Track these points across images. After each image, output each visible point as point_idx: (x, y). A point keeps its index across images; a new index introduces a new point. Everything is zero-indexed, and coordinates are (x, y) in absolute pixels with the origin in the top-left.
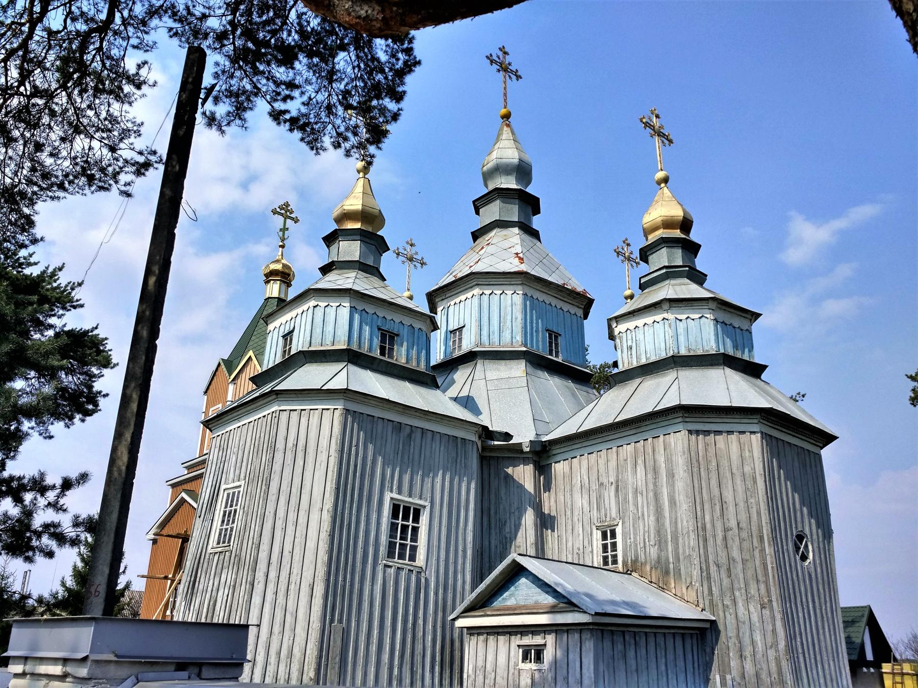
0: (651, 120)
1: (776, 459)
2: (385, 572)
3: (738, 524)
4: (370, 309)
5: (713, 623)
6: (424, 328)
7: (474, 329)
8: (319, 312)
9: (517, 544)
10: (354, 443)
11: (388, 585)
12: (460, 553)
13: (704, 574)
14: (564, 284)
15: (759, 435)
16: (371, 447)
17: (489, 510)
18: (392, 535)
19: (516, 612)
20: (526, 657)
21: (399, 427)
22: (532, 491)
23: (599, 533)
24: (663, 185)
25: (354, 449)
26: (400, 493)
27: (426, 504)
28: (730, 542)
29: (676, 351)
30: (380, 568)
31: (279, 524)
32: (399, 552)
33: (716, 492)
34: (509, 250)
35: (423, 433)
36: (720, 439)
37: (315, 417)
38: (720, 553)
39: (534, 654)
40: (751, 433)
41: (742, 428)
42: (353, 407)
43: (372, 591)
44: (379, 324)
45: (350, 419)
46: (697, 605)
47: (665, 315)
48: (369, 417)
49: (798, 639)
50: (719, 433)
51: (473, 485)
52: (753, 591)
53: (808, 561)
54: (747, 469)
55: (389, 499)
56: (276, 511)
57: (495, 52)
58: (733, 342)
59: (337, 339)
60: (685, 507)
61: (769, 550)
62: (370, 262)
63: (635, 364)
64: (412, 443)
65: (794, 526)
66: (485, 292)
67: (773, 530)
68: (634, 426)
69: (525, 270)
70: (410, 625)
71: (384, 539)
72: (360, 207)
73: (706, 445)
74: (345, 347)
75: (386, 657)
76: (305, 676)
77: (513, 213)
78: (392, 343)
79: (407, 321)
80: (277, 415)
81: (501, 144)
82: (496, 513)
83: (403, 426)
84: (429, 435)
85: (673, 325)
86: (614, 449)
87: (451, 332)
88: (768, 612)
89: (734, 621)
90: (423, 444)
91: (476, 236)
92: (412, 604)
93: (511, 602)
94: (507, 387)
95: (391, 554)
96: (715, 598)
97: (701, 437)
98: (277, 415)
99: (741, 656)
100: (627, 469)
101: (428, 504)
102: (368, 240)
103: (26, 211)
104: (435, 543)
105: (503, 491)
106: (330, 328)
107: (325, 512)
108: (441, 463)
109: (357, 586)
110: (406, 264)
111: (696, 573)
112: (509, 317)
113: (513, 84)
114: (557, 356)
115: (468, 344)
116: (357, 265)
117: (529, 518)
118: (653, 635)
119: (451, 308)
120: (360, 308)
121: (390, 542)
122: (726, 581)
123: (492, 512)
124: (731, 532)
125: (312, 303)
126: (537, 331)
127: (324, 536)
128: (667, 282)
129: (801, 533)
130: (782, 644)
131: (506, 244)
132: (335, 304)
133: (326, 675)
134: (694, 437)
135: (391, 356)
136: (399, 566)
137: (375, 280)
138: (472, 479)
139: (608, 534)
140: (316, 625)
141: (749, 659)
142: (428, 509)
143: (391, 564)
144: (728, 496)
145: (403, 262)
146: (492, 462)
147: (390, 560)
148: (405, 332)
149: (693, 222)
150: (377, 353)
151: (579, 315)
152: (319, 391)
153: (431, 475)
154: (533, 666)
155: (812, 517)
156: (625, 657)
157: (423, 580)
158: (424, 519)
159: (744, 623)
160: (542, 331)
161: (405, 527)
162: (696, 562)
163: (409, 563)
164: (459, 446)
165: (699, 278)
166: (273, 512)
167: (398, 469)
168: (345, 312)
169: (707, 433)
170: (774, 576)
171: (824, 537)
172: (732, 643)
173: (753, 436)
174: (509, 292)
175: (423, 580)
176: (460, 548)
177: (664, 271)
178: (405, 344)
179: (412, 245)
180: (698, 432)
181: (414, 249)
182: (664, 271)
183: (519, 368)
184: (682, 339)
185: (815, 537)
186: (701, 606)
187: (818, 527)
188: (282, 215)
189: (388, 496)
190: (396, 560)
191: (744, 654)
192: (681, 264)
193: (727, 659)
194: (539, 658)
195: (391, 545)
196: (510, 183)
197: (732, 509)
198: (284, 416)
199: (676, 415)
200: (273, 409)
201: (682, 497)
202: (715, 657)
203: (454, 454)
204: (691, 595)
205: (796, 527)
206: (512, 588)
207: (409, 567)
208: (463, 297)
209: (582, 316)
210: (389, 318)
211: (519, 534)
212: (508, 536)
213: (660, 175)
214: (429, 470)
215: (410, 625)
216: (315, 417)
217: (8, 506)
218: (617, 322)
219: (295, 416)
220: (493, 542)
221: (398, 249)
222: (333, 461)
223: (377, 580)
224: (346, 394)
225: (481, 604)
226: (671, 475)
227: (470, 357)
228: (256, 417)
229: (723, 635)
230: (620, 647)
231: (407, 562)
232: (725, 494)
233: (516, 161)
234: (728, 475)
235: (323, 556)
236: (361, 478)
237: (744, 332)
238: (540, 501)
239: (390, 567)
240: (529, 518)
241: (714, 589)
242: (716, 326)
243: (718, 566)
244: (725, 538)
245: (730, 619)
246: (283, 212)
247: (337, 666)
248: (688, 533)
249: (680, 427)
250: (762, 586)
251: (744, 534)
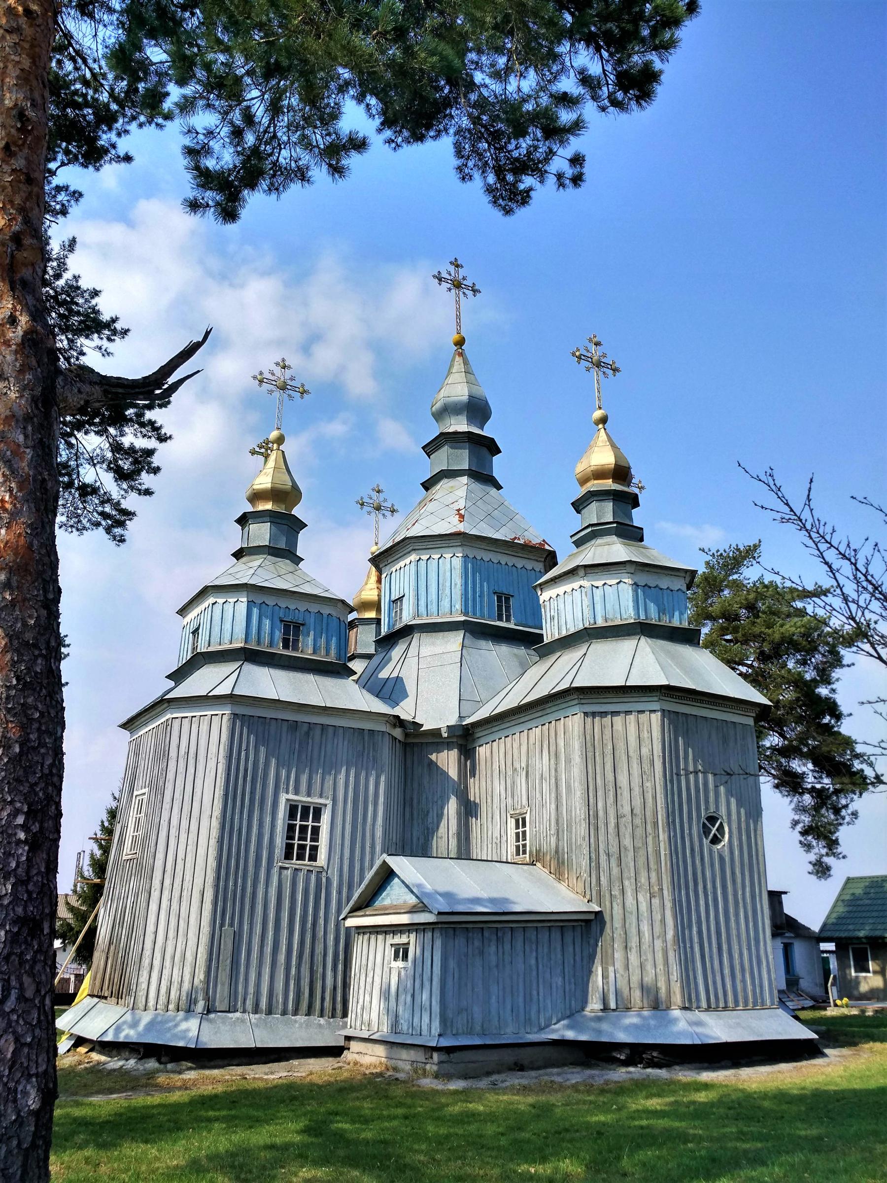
0: (588, 351)
1: (683, 738)
2: (280, 874)
3: (632, 810)
4: (271, 601)
5: (598, 914)
6: (334, 613)
7: (412, 600)
8: (218, 609)
9: (439, 835)
10: (244, 747)
11: (284, 886)
12: (368, 849)
13: (593, 864)
14: (515, 538)
15: (659, 714)
16: (262, 749)
17: (412, 799)
18: (290, 837)
19: (387, 912)
20: (396, 956)
21: (294, 726)
22: (456, 778)
23: (513, 821)
24: (601, 426)
25: (243, 753)
26: (297, 792)
27: (327, 802)
28: (622, 829)
29: (592, 621)
30: (275, 871)
31: (173, 832)
32: (297, 853)
33: (610, 776)
34: (451, 506)
35: (322, 730)
36: (618, 720)
37: (205, 723)
38: (611, 841)
39: (401, 952)
40: (651, 711)
41: (640, 707)
42: (241, 710)
43: (266, 892)
44: (281, 615)
45: (238, 723)
46: (584, 896)
47: (582, 583)
48: (261, 720)
49: (695, 929)
50: (616, 713)
51: (383, 778)
52: (643, 880)
53: (723, 843)
54: (645, 751)
55: (284, 801)
56: (170, 820)
57: (453, 260)
58: (658, 606)
59: (235, 637)
60: (578, 794)
61: (663, 836)
62: (282, 545)
63: (557, 637)
64: (310, 741)
65: (703, 807)
66: (422, 557)
67: (670, 815)
68: (539, 708)
69: (462, 530)
70: (309, 925)
71: (280, 841)
72: (269, 486)
73: (602, 727)
74: (242, 645)
75: (282, 958)
76: (196, 979)
77: (463, 459)
78: (297, 634)
79: (314, 608)
80: (168, 724)
81: (450, 380)
82: (419, 802)
83: (299, 724)
84: (331, 730)
85: (590, 592)
86: (526, 731)
87: (393, 602)
88: (658, 901)
89: (621, 911)
90: (324, 742)
91: (427, 485)
92: (311, 904)
93: (387, 902)
94: (439, 664)
95: (288, 856)
96: (603, 889)
97: (597, 719)
98: (168, 724)
99: (626, 947)
101: (329, 802)
102: (279, 521)
103: (352, 92)
104: (338, 841)
105: (426, 781)
106: (227, 626)
107: (214, 819)
108: (344, 758)
109: (249, 890)
110: (373, 515)
111: (585, 863)
112: (448, 584)
113: (468, 302)
114: (508, 620)
115: (407, 617)
116: (266, 550)
117: (452, 806)
118: (522, 929)
119: (393, 574)
120: (259, 601)
121: (287, 844)
122: (615, 871)
123: (415, 801)
124: (624, 819)
125: (211, 600)
126: (481, 596)
127: (213, 842)
128: (593, 542)
129: (715, 815)
130: (670, 934)
131: (450, 499)
132: (232, 600)
133: (217, 977)
134: (589, 720)
135: (296, 648)
136: (297, 867)
137: (285, 565)
138: (382, 772)
139: (520, 822)
140: (206, 929)
141: (634, 950)
142: (329, 807)
143: (287, 866)
144: (623, 780)
146: (416, 749)
147: (287, 861)
148: (311, 621)
149: (629, 468)
150: (279, 650)
151: (537, 570)
153: (333, 772)
154: (400, 964)
155: (732, 796)
156: (482, 953)
157: (324, 880)
158: (326, 818)
159: (631, 913)
160: (489, 595)
161: (303, 829)
162: (586, 851)
163: (309, 863)
164: (366, 738)
165: (633, 535)
166: (167, 820)
167: (294, 770)
168: (242, 607)
169: (603, 714)
170: (666, 863)
171: (748, 815)
172: (618, 933)
173: (653, 716)
174: (448, 556)
175: (324, 880)
176: (368, 845)
177: (589, 530)
178: (312, 633)
179: (378, 492)
180: (594, 715)
181: (382, 496)
182: (589, 530)
183: (454, 641)
184: (599, 608)
185: (734, 817)
186: (588, 897)
187: (739, 805)
188: (262, 454)
189: (283, 798)
190: (294, 861)
191: (629, 945)
192: (611, 520)
193: (610, 951)
194: (405, 957)
195: (289, 848)
196: (460, 425)
197: (626, 794)
198: (176, 724)
199: (572, 697)
200: (167, 717)
201: (576, 784)
202: (599, 949)
203: (360, 748)
204: (580, 888)
205: (707, 809)
206: (389, 888)
207: (308, 868)
208: (402, 564)
209: (542, 571)
210: (292, 607)
211: (442, 825)
212: (430, 826)
213: (598, 414)
214: (331, 767)
215: (309, 925)
216: (205, 723)
218: (541, 590)
219: (186, 722)
220: (414, 834)
221: (362, 498)
222: (221, 767)
223: (272, 883)
224: (231, 698)
225: (365, 904)
226: (568, 761)
227: (407, 631)
228: (157, 724)
229: (608, 926)
230: (477, 943)
231: (306, 862)
232: (619, 778)
233: (465, 398)
234: (624, 758)
235: (212, 863)
236: (252, 782)
238: (466, 787)
239: (287, 868)
240: (452, 806)
241: (602, 879)
242: (635, 592)
243: (608, 855)
244: (617, 826)
245: (617, 910)
246: (263, 450)
247: (228, 968)
248: (580, 820)
249: (576, 710)
250: (653, 875)
251: (638, 821)
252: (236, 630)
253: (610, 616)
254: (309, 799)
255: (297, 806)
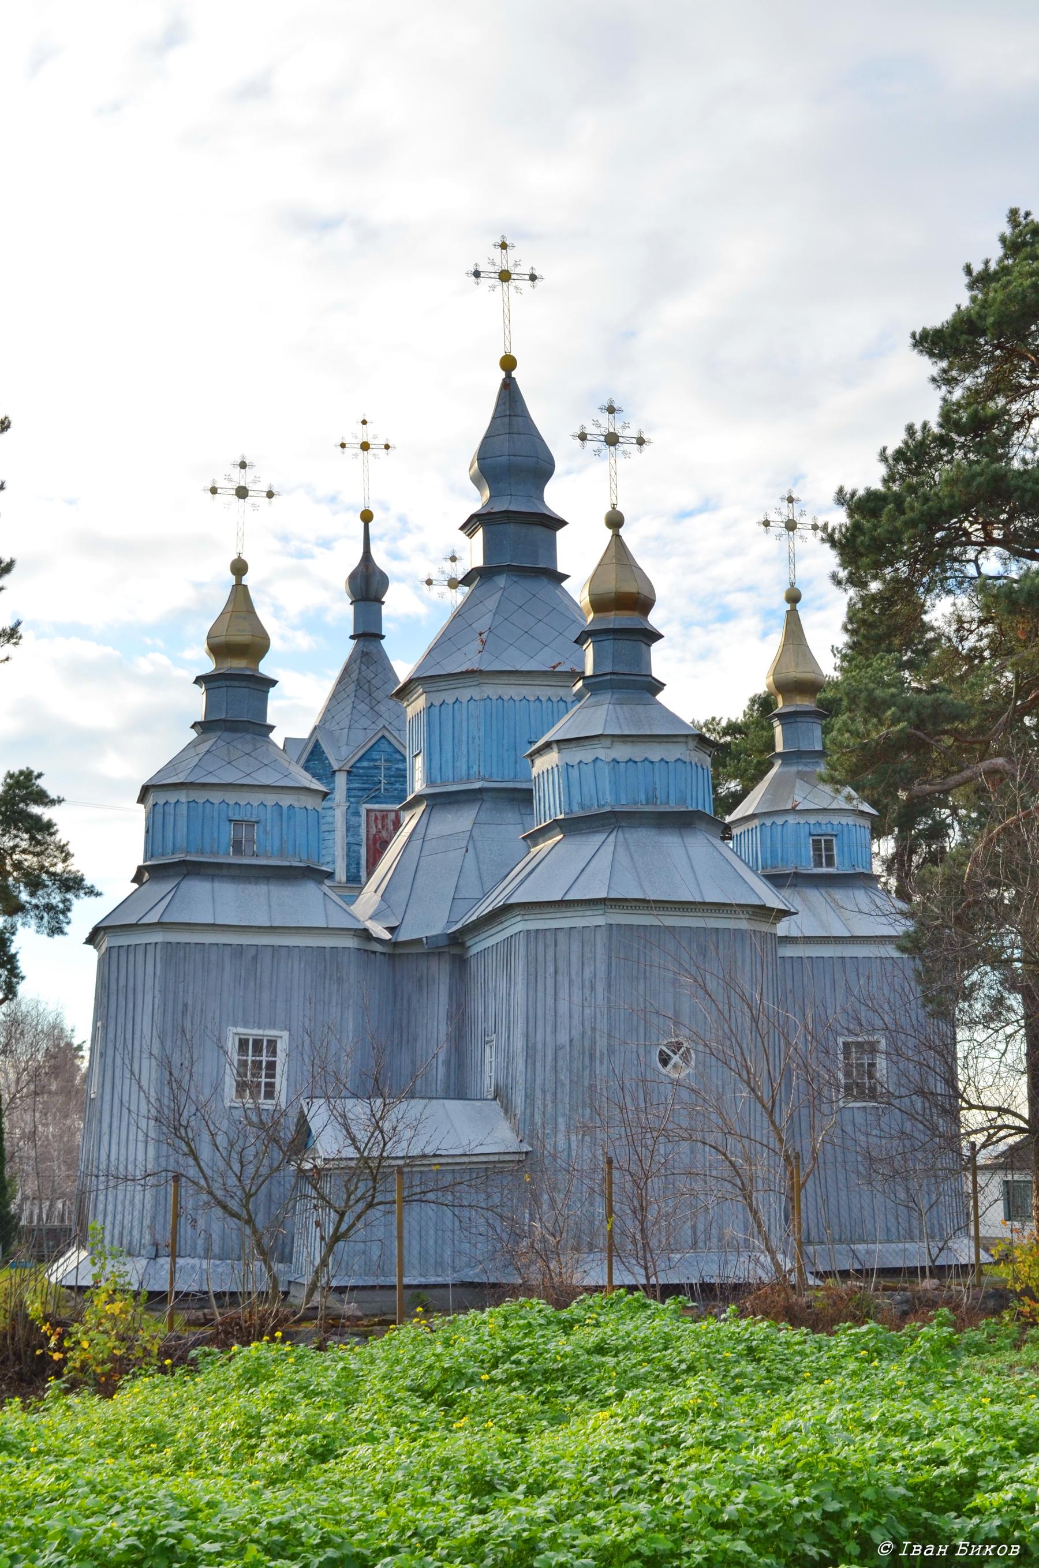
64: (259, 966)
79: (270, 799)
90: (275, 966)
100: (260, 1091)
124: (563, 1051)
145: (493, 287)
152: (136, 925)
217: (49, 1555)
237: (672, 766)
252: (179, 838)
253: (587, 802)
254: (261, 1032)
255: (247, 1040)
